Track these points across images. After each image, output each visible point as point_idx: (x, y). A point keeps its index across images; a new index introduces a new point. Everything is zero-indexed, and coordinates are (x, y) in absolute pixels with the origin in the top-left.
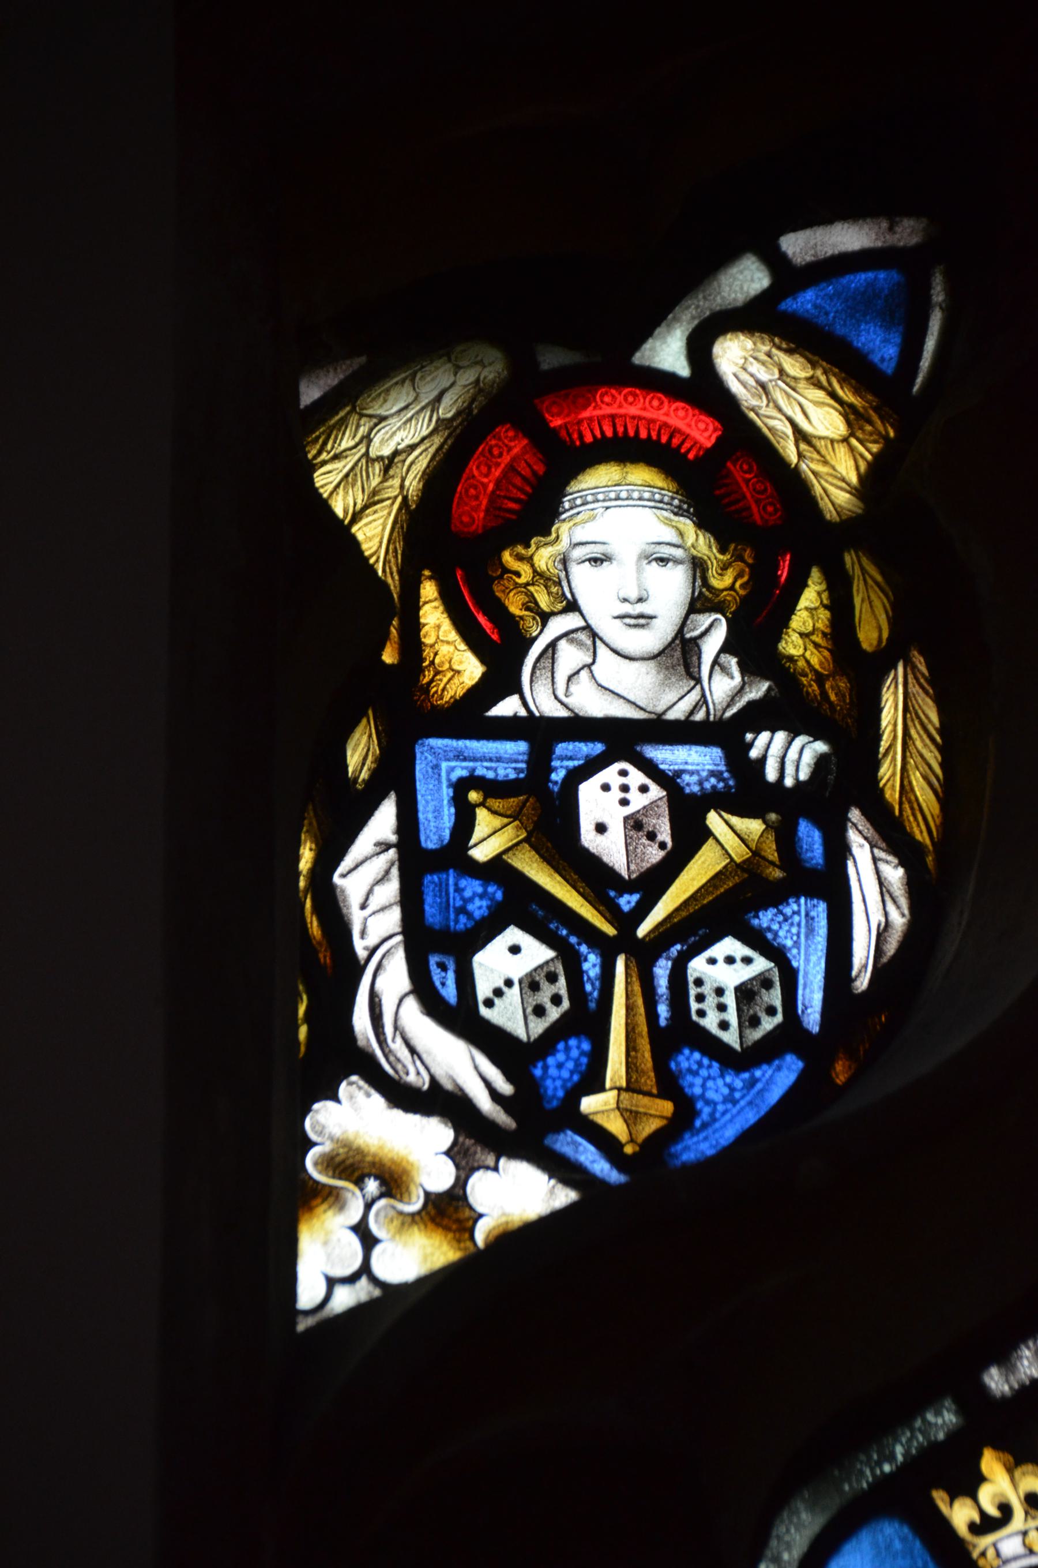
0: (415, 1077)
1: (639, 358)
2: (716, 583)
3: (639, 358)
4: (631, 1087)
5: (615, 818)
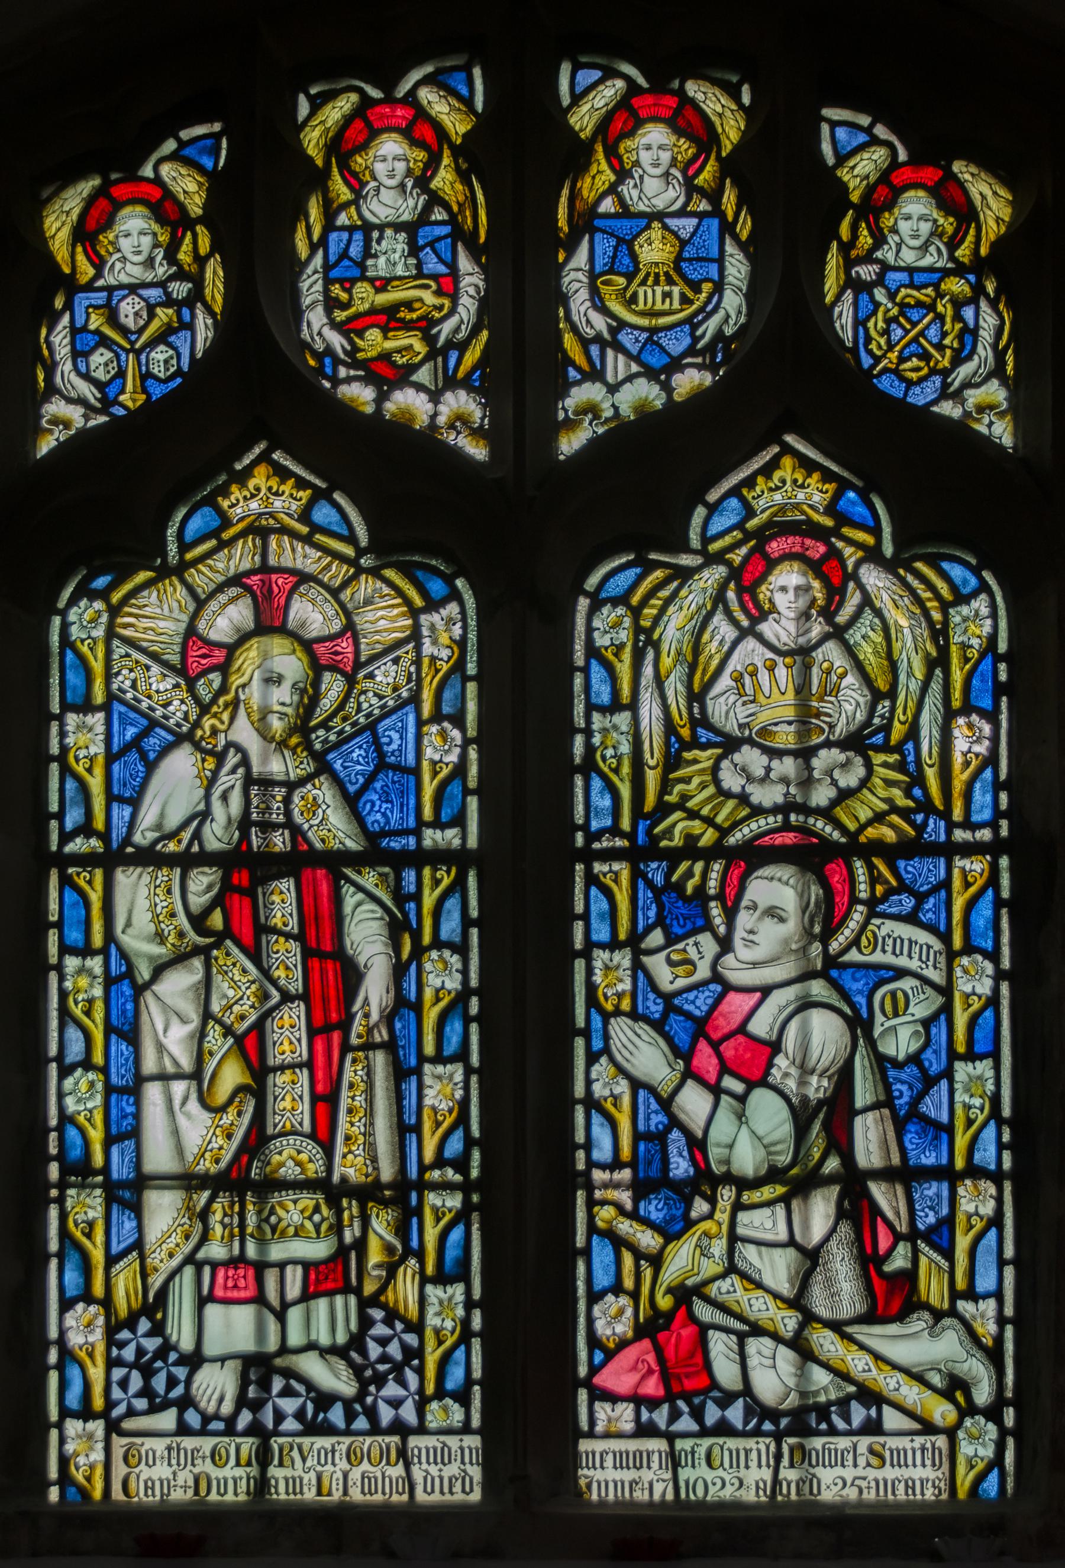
0: (74, 394)
1: (140, 173)
2: (161, 239)
3: (140, 173)
4: (135, 392)
5: (131, 311)
